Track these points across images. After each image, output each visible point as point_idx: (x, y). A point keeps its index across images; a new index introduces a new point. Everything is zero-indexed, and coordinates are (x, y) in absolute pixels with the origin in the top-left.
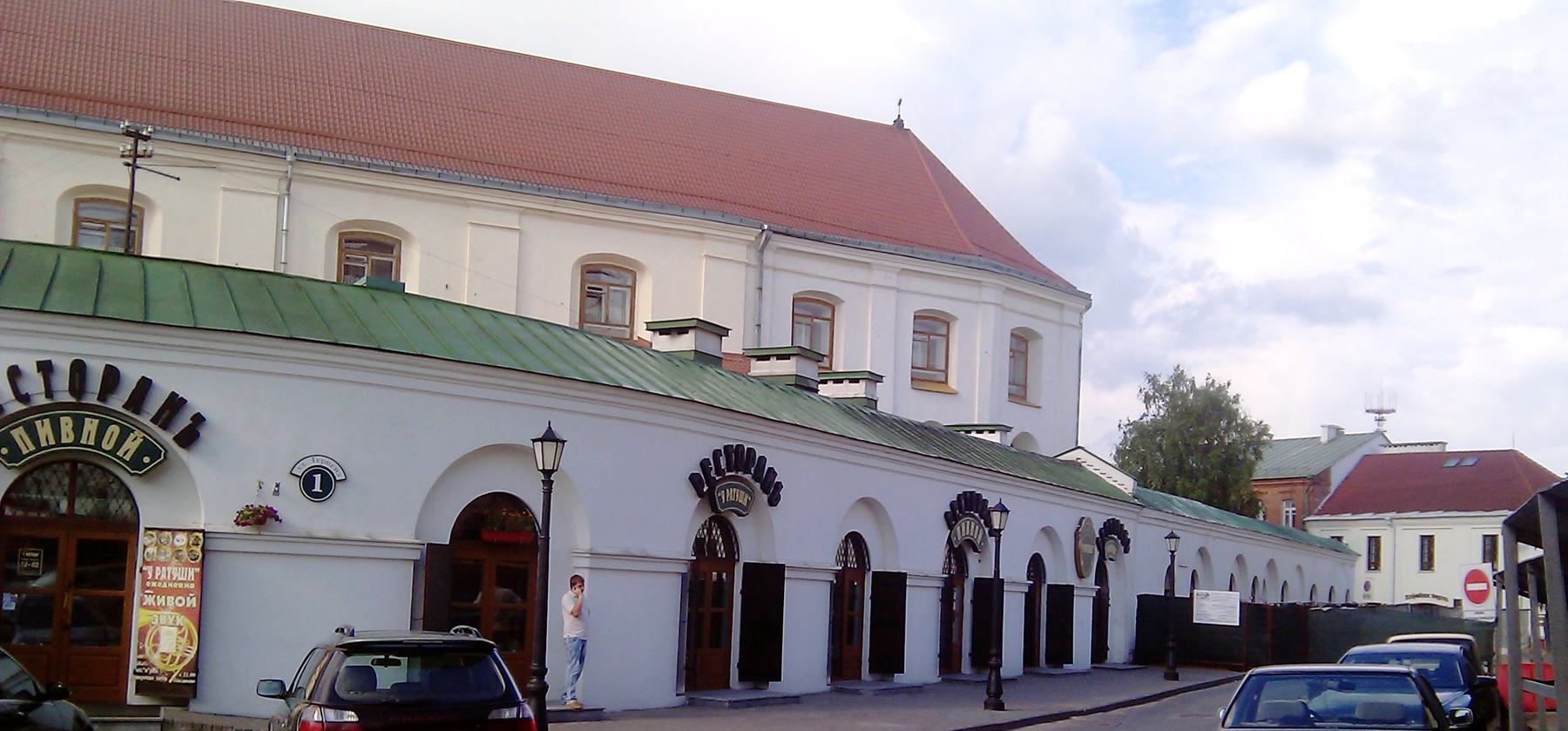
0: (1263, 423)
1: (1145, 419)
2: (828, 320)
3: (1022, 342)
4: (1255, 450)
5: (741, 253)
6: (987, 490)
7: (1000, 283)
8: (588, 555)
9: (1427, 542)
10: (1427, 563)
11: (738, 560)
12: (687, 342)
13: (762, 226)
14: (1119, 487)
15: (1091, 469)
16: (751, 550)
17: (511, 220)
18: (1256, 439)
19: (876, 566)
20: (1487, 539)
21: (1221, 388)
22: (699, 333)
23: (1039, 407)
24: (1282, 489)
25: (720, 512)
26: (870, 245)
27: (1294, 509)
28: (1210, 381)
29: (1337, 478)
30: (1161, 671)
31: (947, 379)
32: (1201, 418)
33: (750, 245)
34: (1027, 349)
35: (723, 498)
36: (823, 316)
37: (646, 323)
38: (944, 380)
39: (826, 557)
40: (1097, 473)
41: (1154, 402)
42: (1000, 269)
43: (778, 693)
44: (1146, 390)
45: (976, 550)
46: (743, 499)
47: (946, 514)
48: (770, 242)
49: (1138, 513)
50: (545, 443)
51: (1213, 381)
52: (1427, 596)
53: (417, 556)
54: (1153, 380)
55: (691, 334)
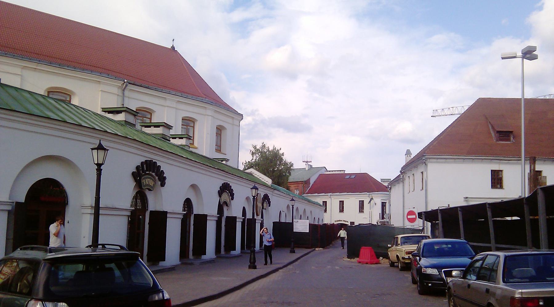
0: (292, 163)
1: (252, 161)
2: (149, 118)
3: (220, 130)
4: (289, 172)
5: (115, 90)
6: (232, 182)
7: (213, 108)
8: (90, 208)
9: (342, 203)
10: (342, 210)
11: (148, 210)
12: (121, 117)
13: (124, 81)
14: (266, 182)
15: (256, 176)
16: (153, 205)
17: (18, 71)
18: (289, 168)
19: (195, 212)
20: (324, 202)
21: (278, 151)
22: (128, 114)
23: (226, 154)
24: (295, 185)
25: (143, 189)
26: (167, 91)
27: (299, 192)
28: (274, 148)
29: (312, 182)
30: (289, 250)
31: (193, 143)
32: (271, 161)
33: (119, 87)
34: (221, 133)
35: (144, 183)
36: (147, 117)
37: (102, 108)
38: (192, 143)
39: (179, 208)
40: (258, 177)
41: (255, 155)
42: (213, 103)
43: (166, 266)
44: (252, 151)
45: (227, 205)
46: (152, 183)
47: (219, 191)
48: (127, 87)
49: (273, 192)
50: (99, 151)
51: (275, 148)
52: (342, 221)
53: (9, 208)
54: (255, 147)
55: (123, 114)
